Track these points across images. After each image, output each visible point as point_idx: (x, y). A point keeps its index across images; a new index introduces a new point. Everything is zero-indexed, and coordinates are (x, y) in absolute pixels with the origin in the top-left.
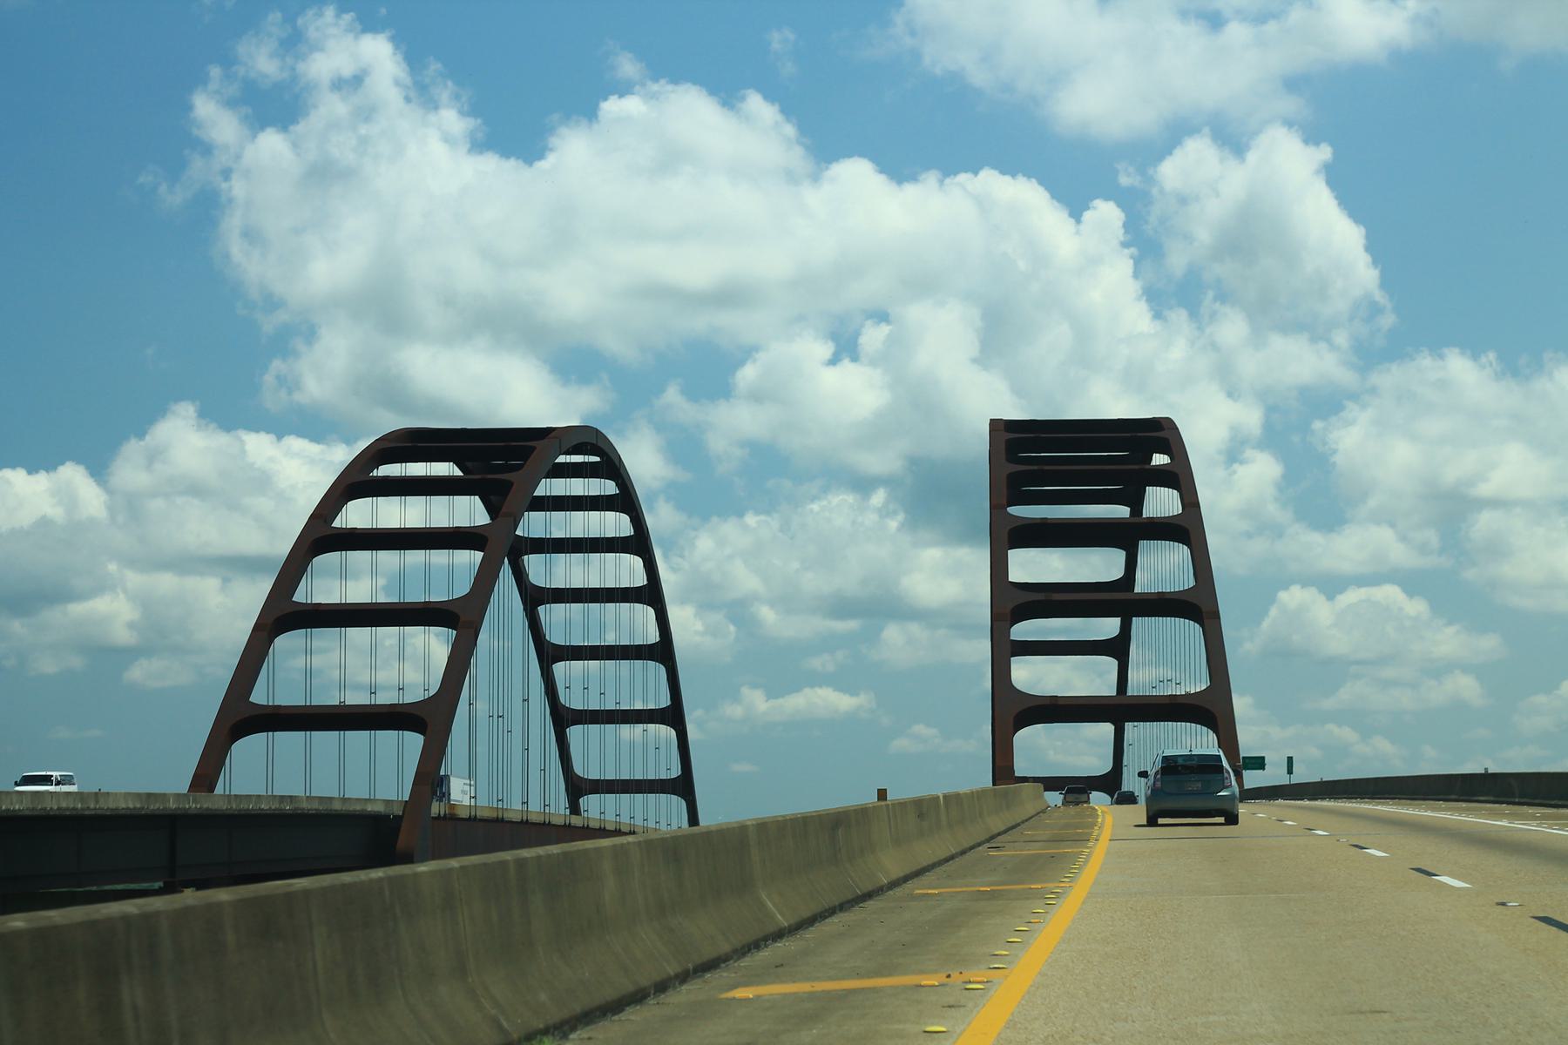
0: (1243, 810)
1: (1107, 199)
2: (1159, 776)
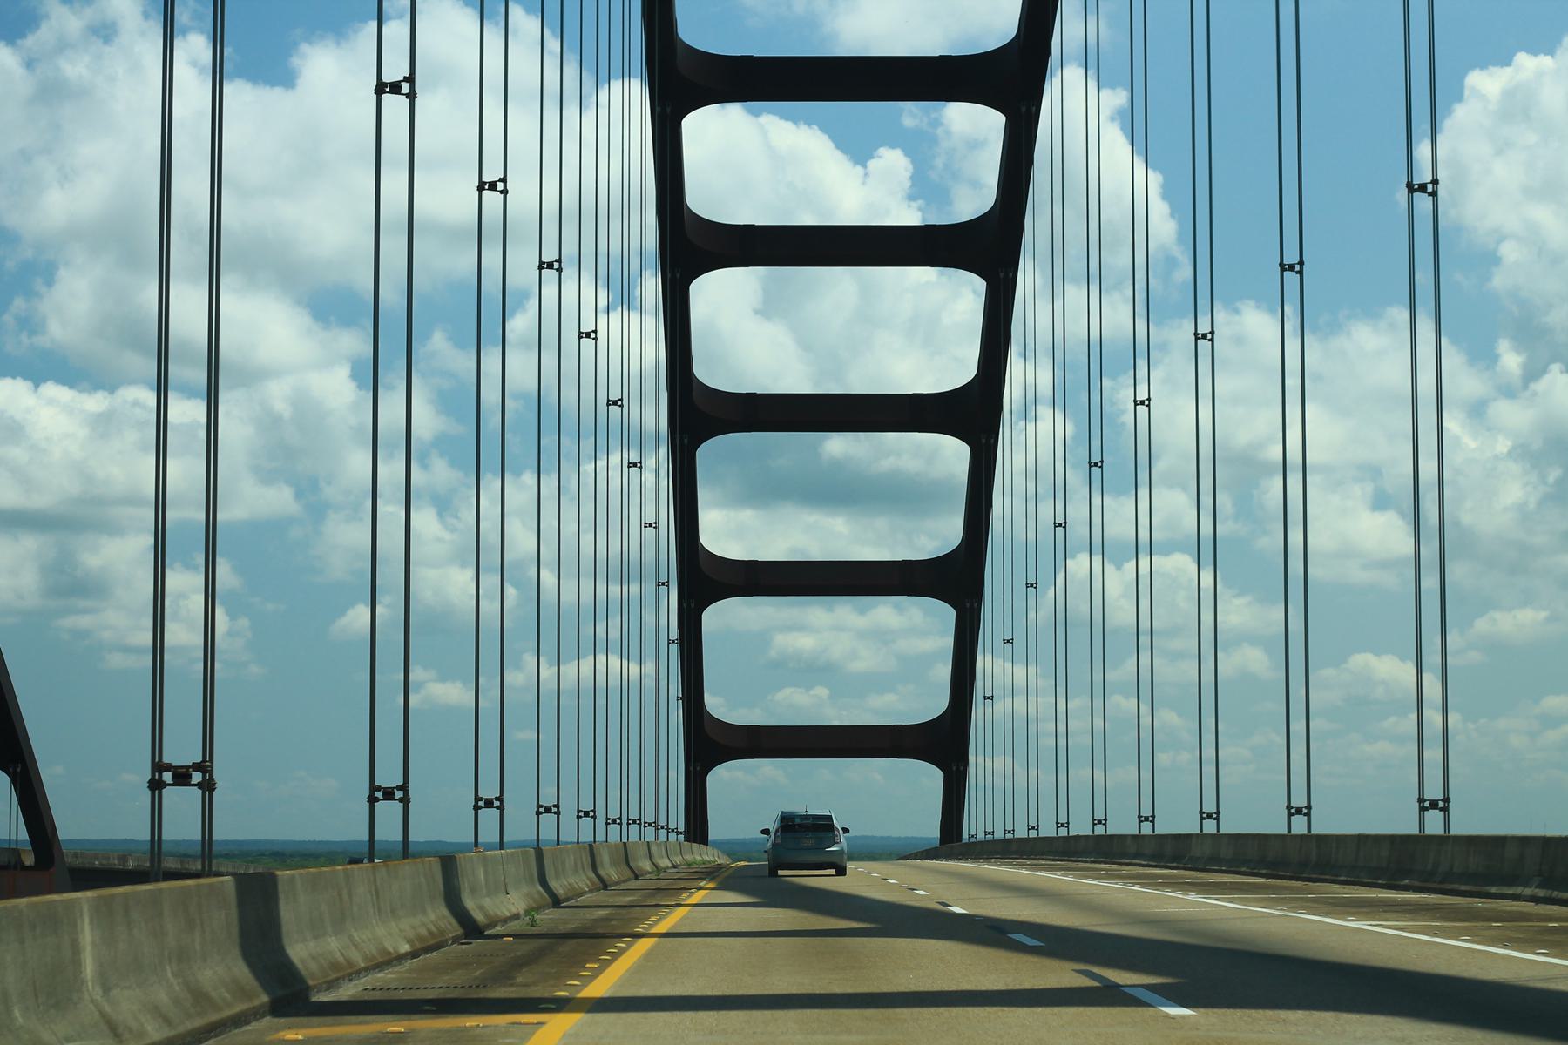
0: (851, 866)
1: (893, 147)
2: (779, 834)
